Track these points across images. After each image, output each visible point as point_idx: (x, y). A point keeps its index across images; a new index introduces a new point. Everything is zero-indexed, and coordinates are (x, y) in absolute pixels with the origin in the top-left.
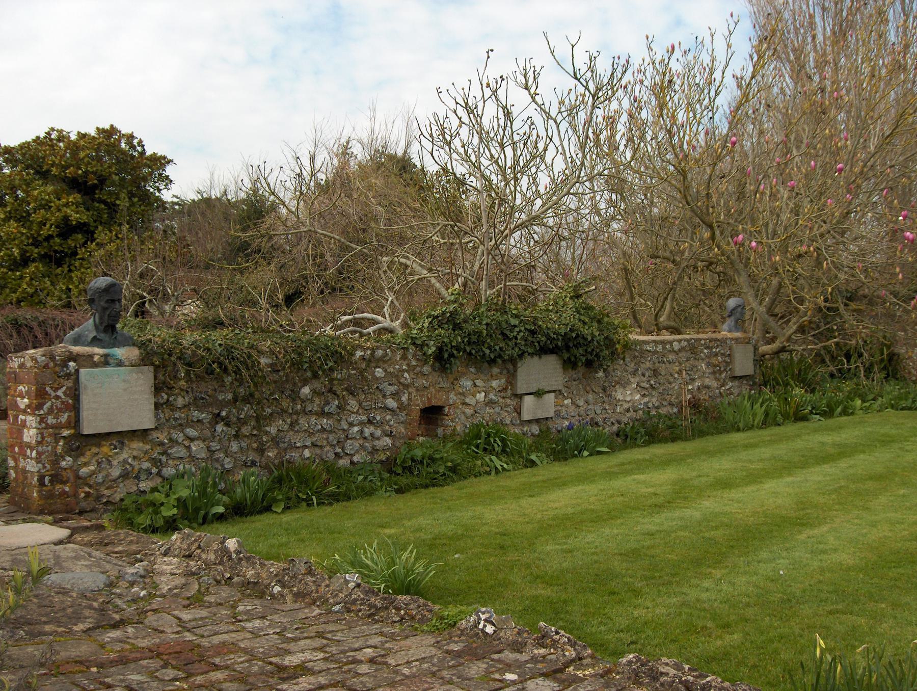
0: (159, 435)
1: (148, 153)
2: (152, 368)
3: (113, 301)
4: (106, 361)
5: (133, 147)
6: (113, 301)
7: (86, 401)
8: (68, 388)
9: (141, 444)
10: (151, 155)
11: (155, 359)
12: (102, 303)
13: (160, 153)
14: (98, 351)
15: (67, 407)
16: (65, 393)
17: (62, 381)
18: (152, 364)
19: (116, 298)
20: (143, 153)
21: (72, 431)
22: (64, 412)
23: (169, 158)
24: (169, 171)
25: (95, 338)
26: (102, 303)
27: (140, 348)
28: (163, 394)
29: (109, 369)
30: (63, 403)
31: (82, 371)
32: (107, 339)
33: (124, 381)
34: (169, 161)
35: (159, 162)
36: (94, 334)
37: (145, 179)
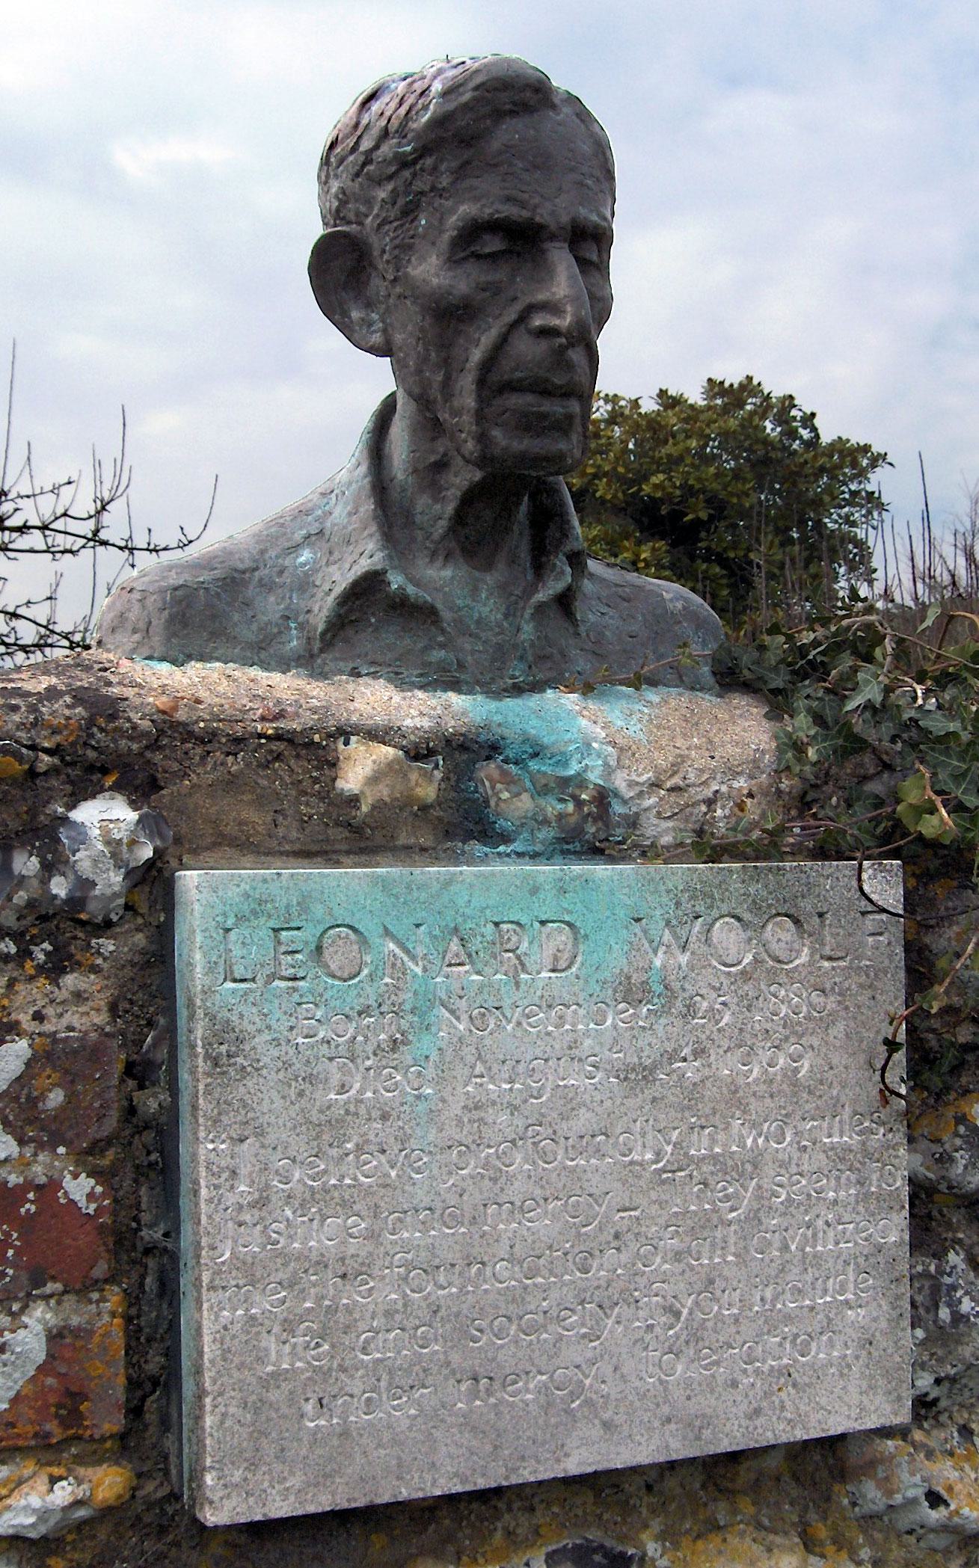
1: (826, 438)
2: (885, 884)
4: (457, 802)
7: (242, 1197)
8: (49, 1055)
10: (832, 445)
12: (429, 269)
14: (389, 701)
18: (892, 839)
19: (556, 208)
20: (814, 443)
21: (108, 1482)
23: (876, 449)
24: (878, 480)
25: (365, 591)
26: (429, 269)
27: (778, 704)
29: (480, 882)
32: (488, 608)
33: (632, 992)
34: (878, 460)
35: (856, 458)
36: (365, 556)
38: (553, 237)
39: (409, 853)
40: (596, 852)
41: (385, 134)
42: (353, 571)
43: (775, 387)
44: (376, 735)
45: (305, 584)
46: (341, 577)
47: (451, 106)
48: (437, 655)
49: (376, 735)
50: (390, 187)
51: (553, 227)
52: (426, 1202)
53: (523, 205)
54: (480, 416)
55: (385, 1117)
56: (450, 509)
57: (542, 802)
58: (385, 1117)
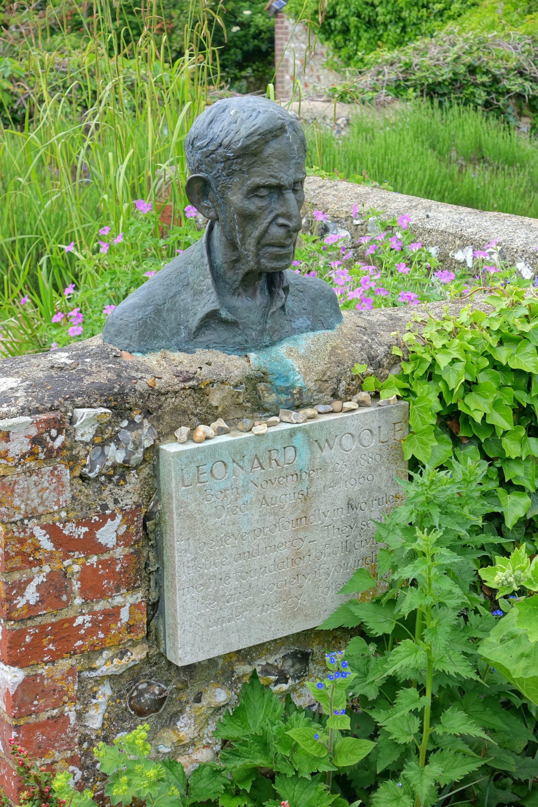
25: (212, 317)
26: (236, 198)
36: (209, 302)
38: (286, 189)
41: (221, 145)
42: (206, 307)
46: (202, 311)
47: (248, 142)
48: (239, 339)
50: (223, 165)
51: (287, 185)
52: (247, 550)
53: (276, 178)
54: (257, 255)
55: (233, 524)
56: (240, 277)
57: (280, 396)
58: (233, 524)
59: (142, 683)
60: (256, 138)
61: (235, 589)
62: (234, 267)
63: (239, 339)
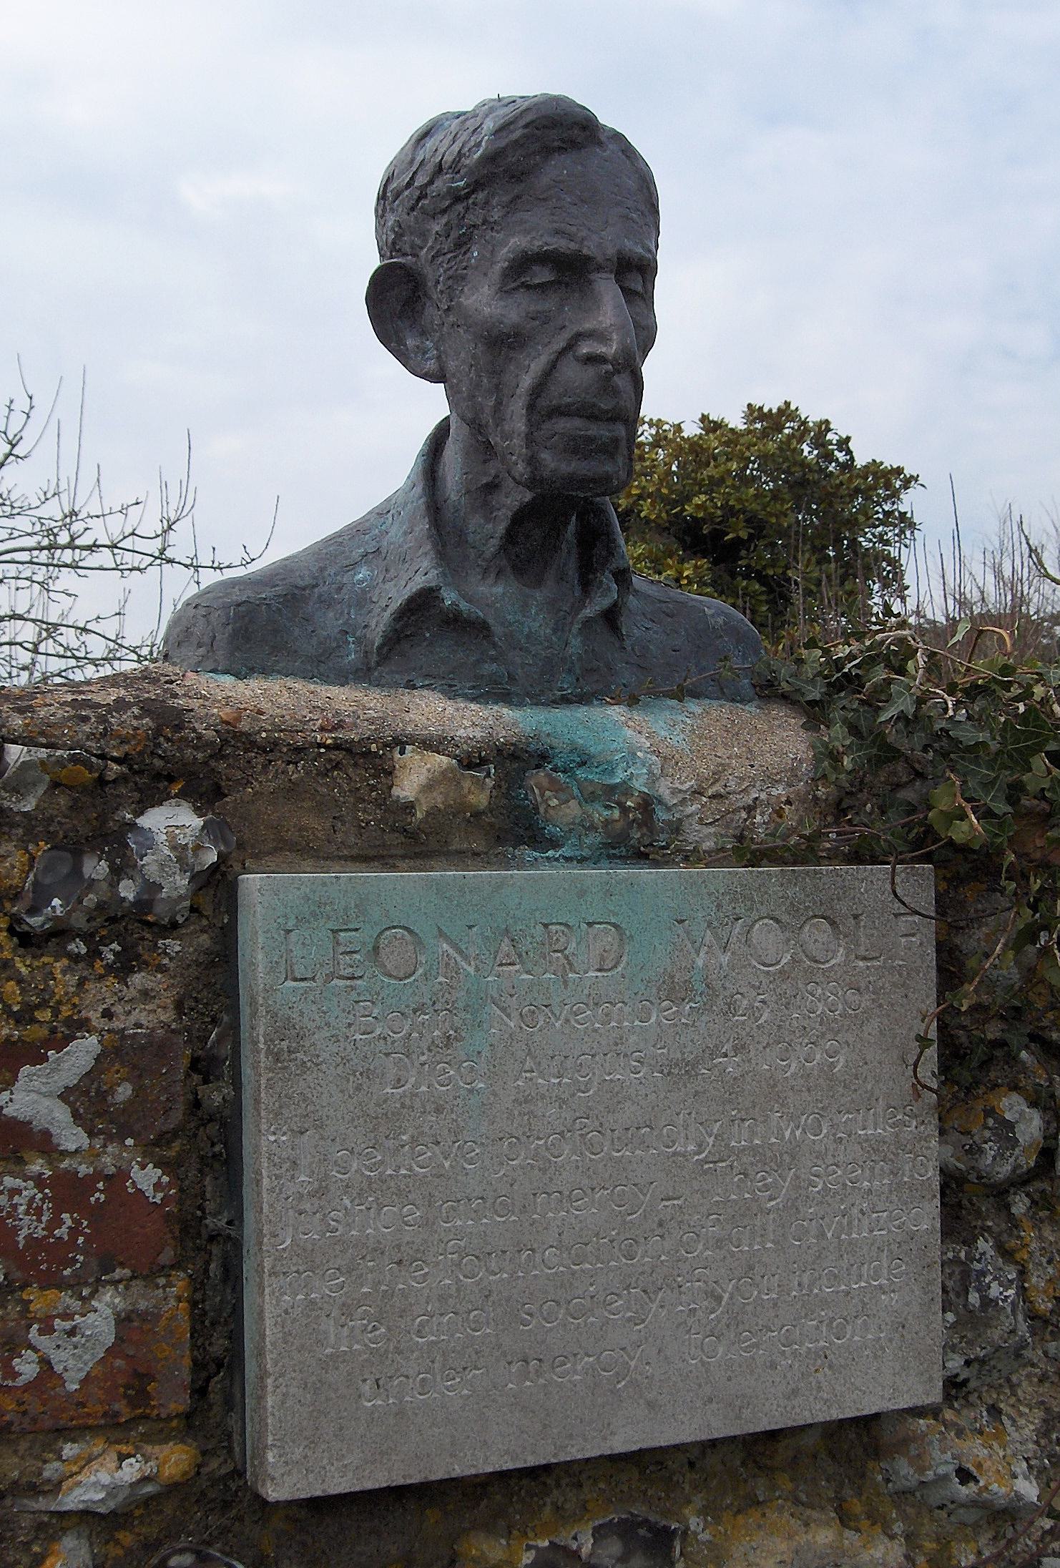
0: (974, 1450)
1: (860, 462)
2: (919, 885)
3: (570, 271)
4: (508, 809)
5: (829, 457)
6: (570, 271)
8: (117, 1051)
9: (824, 1536)
11: (946, 798)
13: (889, 462)
15: (108, 1237)
16: (86, 1100)
17: (63, 979)
18: (924, 844)
19: (602, 241)
20: (848, 466)
21: (174, 1459)
22: (84, 1287)
24: (909, 502)
26: (483, 299)
27: (815, 714)
28: (1012, 1106)
29: (531, 884)
30: (67, 1191)
31: (256, 887)
32: (537, 623)
33: (674, 990)
34: (907, 483)
35: (889, 480)
36: (420, 573)
37: (852, 523)
38: (599, 268)
39: (462, 858)
40: (640, 856)
42: (408, 588)
43: (812, 413)
44: (430, 744)
45: (362, 600)
46: (397, 593)
48: (489, 668)
49: (430, 744)
51: (600, 259)
54: (530, 439)
55: (438, 1110)
56: (501, 528)
57: (589, 808)
59: (181, 1551)
60: (518, 134)
61: (442, 1298)
62: (485, 503)
63: (489, 668)
